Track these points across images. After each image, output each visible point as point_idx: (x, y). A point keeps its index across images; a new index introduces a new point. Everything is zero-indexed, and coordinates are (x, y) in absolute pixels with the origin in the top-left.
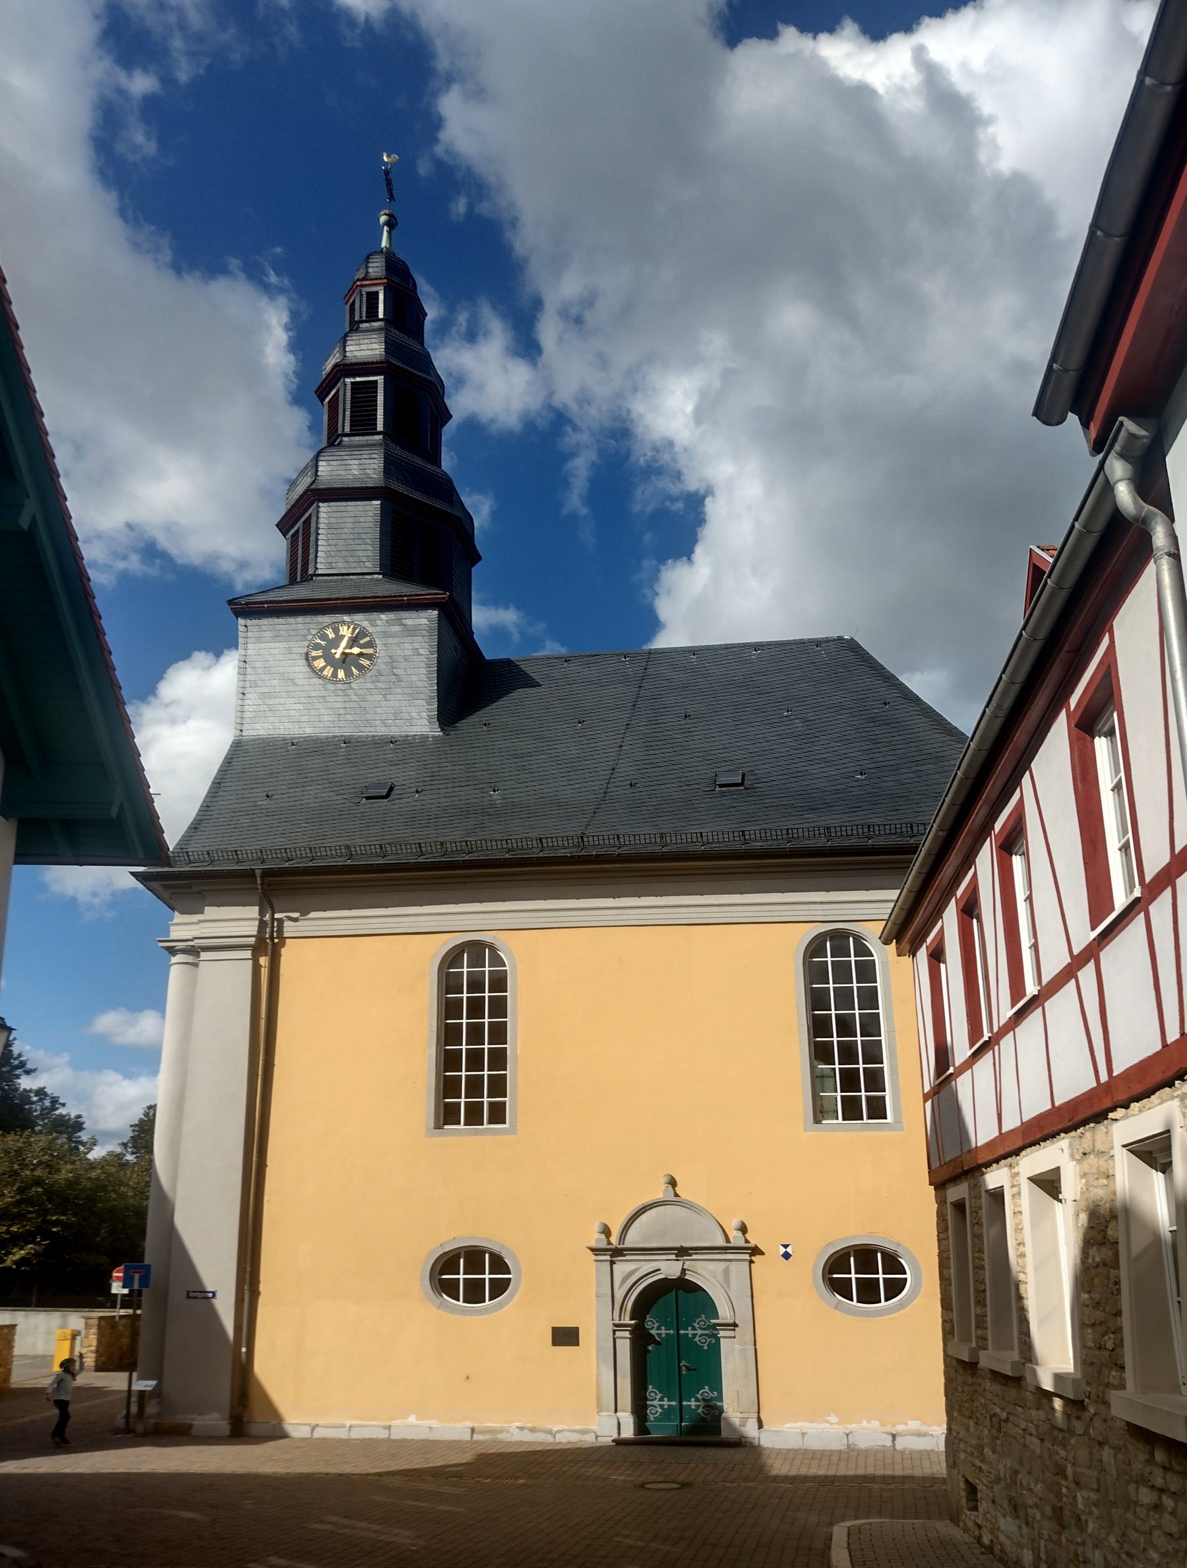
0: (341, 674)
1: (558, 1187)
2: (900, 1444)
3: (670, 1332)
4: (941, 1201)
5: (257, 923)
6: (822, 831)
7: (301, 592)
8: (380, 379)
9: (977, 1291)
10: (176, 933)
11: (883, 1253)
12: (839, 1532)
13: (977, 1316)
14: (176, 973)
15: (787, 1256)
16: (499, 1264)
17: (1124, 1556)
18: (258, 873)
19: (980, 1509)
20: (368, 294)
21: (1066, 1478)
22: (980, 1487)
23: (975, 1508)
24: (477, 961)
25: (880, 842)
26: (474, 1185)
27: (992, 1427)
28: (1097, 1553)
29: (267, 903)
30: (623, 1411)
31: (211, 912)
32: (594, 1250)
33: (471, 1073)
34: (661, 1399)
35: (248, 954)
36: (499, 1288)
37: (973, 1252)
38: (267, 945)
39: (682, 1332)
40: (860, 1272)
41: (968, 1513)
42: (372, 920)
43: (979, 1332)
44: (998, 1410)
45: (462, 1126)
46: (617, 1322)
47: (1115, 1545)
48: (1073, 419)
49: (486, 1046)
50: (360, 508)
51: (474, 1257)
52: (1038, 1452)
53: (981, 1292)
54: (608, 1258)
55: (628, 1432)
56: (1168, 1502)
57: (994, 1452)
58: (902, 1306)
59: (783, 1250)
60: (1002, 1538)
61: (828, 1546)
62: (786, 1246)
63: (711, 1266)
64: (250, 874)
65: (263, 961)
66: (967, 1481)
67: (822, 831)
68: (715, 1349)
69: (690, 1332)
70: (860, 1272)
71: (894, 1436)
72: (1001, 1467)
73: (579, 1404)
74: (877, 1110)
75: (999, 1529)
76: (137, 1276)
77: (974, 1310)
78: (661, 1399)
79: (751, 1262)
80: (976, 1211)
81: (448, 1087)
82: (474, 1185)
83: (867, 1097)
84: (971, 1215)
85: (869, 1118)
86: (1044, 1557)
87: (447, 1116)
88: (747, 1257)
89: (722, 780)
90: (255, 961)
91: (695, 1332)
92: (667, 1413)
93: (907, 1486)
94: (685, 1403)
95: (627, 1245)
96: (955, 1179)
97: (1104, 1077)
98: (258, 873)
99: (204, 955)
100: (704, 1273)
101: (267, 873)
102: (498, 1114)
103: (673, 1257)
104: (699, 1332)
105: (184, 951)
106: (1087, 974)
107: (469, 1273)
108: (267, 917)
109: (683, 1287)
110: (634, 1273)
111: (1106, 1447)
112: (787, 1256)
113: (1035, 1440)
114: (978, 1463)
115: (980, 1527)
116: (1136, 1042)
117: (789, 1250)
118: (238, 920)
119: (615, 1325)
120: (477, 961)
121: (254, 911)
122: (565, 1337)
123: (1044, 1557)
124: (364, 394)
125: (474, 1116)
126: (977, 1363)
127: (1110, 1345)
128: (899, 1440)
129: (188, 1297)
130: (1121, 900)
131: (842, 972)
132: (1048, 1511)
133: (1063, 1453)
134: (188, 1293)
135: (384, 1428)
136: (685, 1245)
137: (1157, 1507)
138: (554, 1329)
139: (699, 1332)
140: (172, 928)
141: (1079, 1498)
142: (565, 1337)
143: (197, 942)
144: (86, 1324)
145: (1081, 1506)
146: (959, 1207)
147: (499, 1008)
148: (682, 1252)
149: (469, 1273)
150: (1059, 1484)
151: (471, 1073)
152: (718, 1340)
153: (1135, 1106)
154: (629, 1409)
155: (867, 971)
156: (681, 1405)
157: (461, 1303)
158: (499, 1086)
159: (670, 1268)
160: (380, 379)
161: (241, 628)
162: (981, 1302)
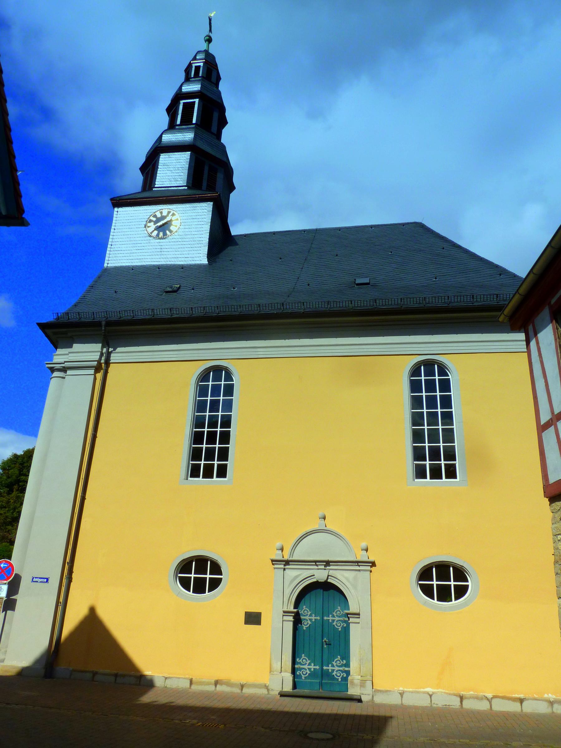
0: (161, 234)
2: (467, 704)
5: (99, 354)
7: (147, 194)
8: (197, 101)
10: (56, 359)
11: (454, 568)
14: (54, 384)
18: (103, 323)
20: (196, 67)
24: (217, 378)
29: (106, 343)
30: (286, 671)
31: (77, 347)
32: (274, 561)
33: (209, 451)
35: (92, 372)
36: (215, 584)
38: (102, 367)
39: (325, 618)
42: (163, 353)
46: (285, 609)
49: (221, 398)
50: (179, 156)
51: (201, 562)
54: (282, 566)
55: (288, 688)
58: (465, 604)
63: (347, 574)
64: (99, 324)
65: (99, 376)
68: (346, 630)
71: (462, 698)
79: (371, 571)
81: (196, 454)
82: (204, 516)
83: (445, 465)
85: (446, 478)
87: (194, 472)
88: (369, 568)
89: (358, 281)
90: (95, 375)
91: (335, 619)
92: (313, 674)
94: (325, 668)
95: (295, 558)
98: (103, 323)
99: (69, 372)
100: (342, 578)
101: (109, 324)
103: (323, 567)
105: (59, 370)
107: (199, 574)
108: (105, 350)
109: (326, 587)
110: (298, 577)
118: (88, 351)
119: (284, 612)
120: (217, 378)
121: (97, 347)
122: (253, 618)
124: (189, 108)
125: (208, 474)
128: (465, 702)
129: (33, 581)
131: (430, 386)
134: (47, 581)
136: (330, 559)
138: (246, 613)
139: (337, 619)
140: (55, 357)
142: (253, 618)
143: (67, 364)
147: (225, 437)
148: (328, 563)
149: (199, 574)
151: (209, 451)
152: (348, 625)
154: (290, 671)
156: (322, 669)
158: (224, 454)
159: (320, 575)
160: (197, 101)
161: (115, 213)
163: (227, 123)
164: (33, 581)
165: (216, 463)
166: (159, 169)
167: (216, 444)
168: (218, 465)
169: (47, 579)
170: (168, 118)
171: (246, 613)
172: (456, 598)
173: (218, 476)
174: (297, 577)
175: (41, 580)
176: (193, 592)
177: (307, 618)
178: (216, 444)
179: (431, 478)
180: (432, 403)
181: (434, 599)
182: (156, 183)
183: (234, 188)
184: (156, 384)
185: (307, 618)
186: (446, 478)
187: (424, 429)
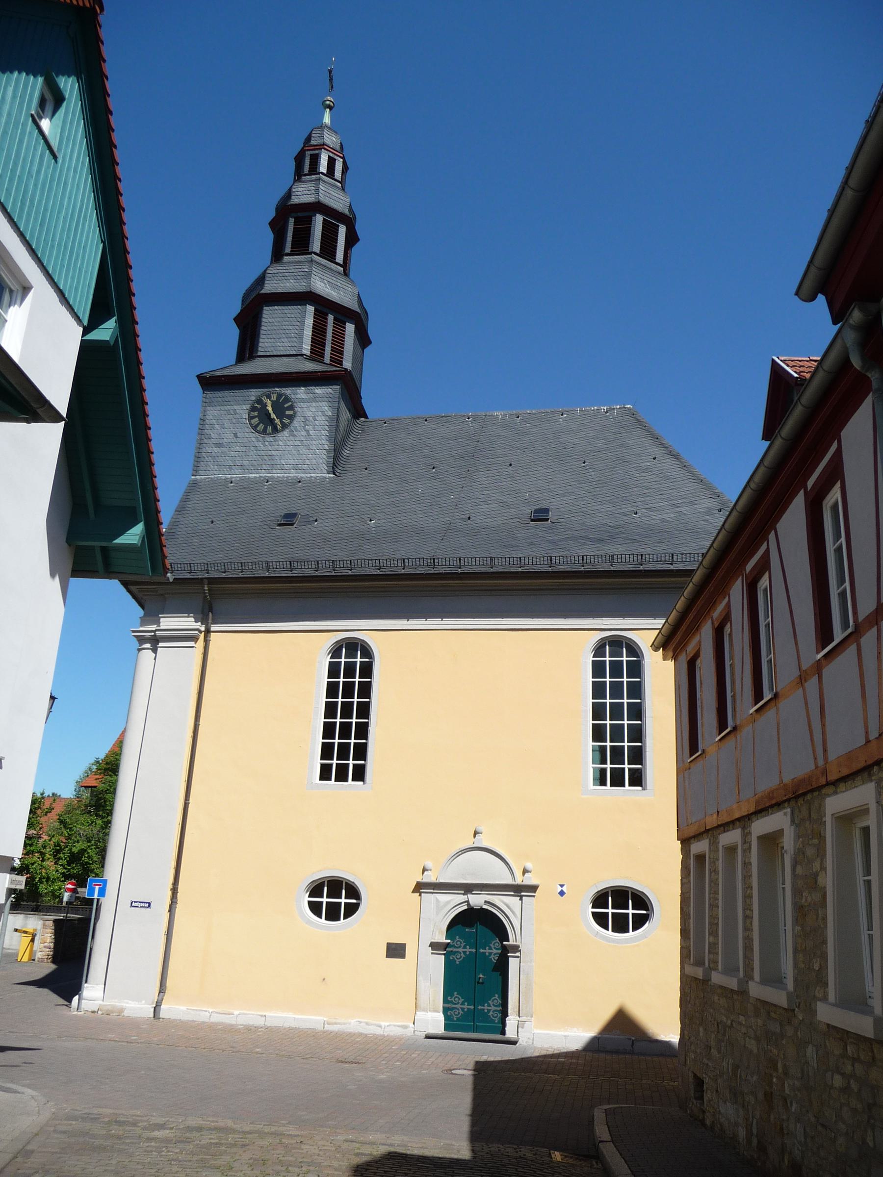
1: (406, 830)
3: (479, 954)
4: (685, 851)
6: (608, 558)
9: (711, 924)
12: (599, 1114)
13: (710, 943)
15: (562, 893)
16: (353, 892)
17: (820, 1128)
19: (706, 1099)
21: (776, 1069)
22: (706, 1080)
23: (701, 1098)
24: (351, 653)
25: (650, 567)
26: (343, 828)
27: (718, 1032)
28: (798, 1125)
33: (345, 750)
34: (463, 1004)
36: (351, 910)
37: (710, 894)
40: (621, 908)
41: (695, 1101)
43: (711, 956)
44: (724, 1019)
45: (608, 787)
47: (813, 1119)
48: (821, 299)
51: (335, 886)
52: (755, 1051)
53: (714, 925)
56: (854, 1085)
57: (719, 1052)
59: (559, 889)
60: (722, 1120)
61: (591, 1121)
62: (562, 886)
66: (695, 1075)
67: (608, 558)
69: (487, 951)
70: (621, 908)
72: (724, 1064)
73: (407, 1004)
74: (637, 779)
75: (720, 1112)
76: (97, 887)
77: (708, 939)
78: (489, 1011)
80: (714, 862)
82: (343, 828)
84: (710, 864)
85: (630, 785)
86: (755, 1131)
93: (644, 1081)
96: (697, 836)
97: (821, 763)
100: (506, 906)
102: (360, 774)
104: (461, 950)
106: (812, 684)
107: (334, 898)
110: (452, 904)
111: (810, 1046)
112: (562, 893)
113: (753, 1042)
114: (705, 1061)
115: (704, 1112)
116: (846, 738)
117: (564, 889)
122: (396, 951)
123: (755, 1131)
125: (342, 776)
126: (710, 980)
127: (816, 967)
129: (131, 906)
130: (839, 635)
132: (761, 1096)
133: (775, 1051)
134: (149, 906)
135: (262, 1016)
137: (846, 1090)
138: (387, 956)
141: (786, 1085)
142: (396, 951)
144: (44, 925)
145: (787, 1091)
146: (700, 858)
149: (334, 898)
150: (771, 1075)
151: (345, 750)
153: (842, 786)
155: (636, 669)
157: (323, 920)
158: (361, 752)
159: (477, 900)
162: (714, 933)
163: (358, 240)
164: (131, 906)
165: (351, 762)
166: (263, 328)
167: (350, 739)
168: (354, 765)
169: (149, 904)
170: (272, 236)
171: (387, 956)
172: (634, 929)
173: (631, 784)
174: (448, 902)
175: (142, 905)
176: (326, 919)
177: (493, 1008)
178: (350, 739)
179: (611, 786)
180: (617, 690)
181: (607, 929)
182: (260, 349)
183: (370, 342)
184: (278, 667)
185: (493, 1008)
186: (630, 785)
187: (322, 897)
